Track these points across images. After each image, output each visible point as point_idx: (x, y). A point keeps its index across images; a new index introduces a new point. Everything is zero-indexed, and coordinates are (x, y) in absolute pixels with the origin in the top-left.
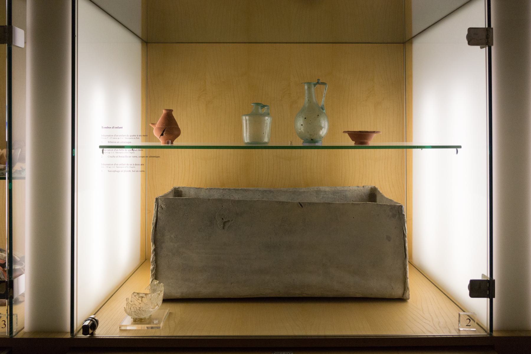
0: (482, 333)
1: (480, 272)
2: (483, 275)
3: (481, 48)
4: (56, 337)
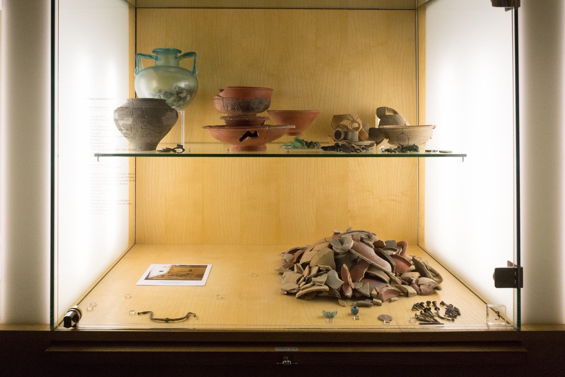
0: (509, 328)
1: (505, 258)
2: (510, 263)
3: (507, 10)
4: (37, 330)
